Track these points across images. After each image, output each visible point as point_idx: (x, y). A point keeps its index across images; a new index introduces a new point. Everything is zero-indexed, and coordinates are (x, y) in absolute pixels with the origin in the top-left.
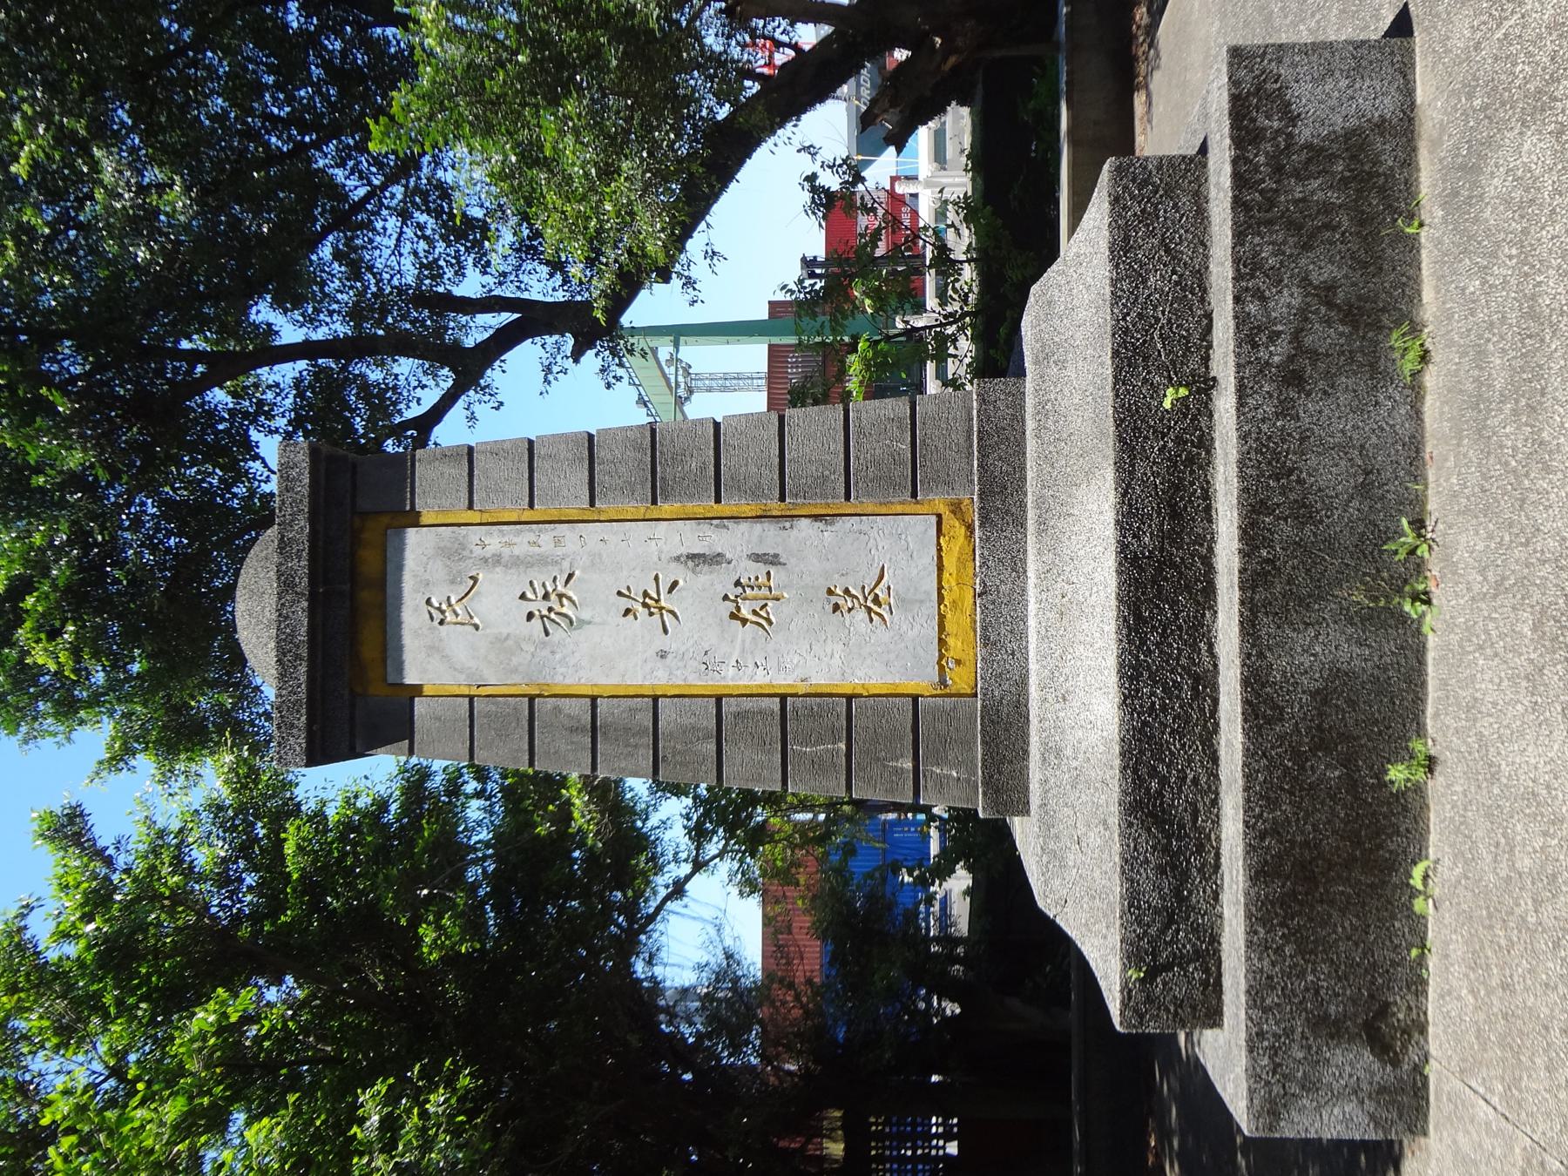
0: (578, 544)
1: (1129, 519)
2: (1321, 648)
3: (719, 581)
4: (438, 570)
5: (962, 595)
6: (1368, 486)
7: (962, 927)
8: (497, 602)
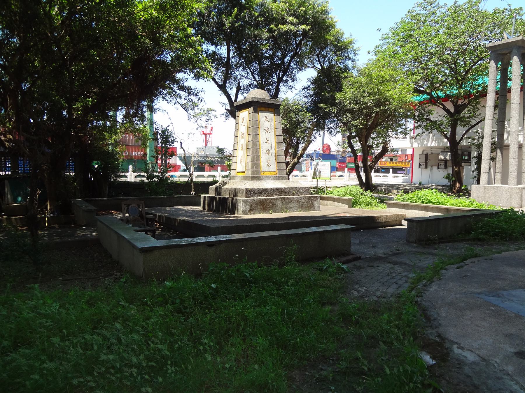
0: (273, 133)
1: (285, 189)
2: (279, 204)
3: (270, 149)
4: (270, 118)
5: (269, 174)
6: (291, 208)
7: (121, 180)
8: (267, 124)
